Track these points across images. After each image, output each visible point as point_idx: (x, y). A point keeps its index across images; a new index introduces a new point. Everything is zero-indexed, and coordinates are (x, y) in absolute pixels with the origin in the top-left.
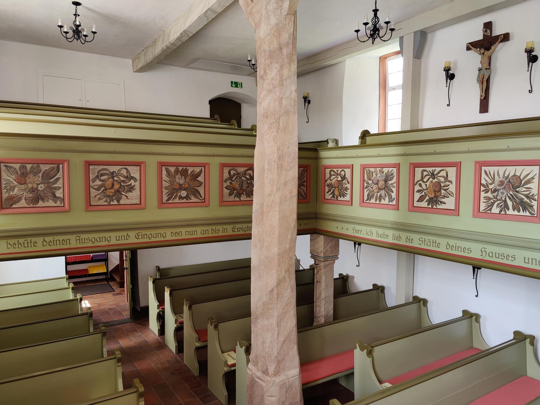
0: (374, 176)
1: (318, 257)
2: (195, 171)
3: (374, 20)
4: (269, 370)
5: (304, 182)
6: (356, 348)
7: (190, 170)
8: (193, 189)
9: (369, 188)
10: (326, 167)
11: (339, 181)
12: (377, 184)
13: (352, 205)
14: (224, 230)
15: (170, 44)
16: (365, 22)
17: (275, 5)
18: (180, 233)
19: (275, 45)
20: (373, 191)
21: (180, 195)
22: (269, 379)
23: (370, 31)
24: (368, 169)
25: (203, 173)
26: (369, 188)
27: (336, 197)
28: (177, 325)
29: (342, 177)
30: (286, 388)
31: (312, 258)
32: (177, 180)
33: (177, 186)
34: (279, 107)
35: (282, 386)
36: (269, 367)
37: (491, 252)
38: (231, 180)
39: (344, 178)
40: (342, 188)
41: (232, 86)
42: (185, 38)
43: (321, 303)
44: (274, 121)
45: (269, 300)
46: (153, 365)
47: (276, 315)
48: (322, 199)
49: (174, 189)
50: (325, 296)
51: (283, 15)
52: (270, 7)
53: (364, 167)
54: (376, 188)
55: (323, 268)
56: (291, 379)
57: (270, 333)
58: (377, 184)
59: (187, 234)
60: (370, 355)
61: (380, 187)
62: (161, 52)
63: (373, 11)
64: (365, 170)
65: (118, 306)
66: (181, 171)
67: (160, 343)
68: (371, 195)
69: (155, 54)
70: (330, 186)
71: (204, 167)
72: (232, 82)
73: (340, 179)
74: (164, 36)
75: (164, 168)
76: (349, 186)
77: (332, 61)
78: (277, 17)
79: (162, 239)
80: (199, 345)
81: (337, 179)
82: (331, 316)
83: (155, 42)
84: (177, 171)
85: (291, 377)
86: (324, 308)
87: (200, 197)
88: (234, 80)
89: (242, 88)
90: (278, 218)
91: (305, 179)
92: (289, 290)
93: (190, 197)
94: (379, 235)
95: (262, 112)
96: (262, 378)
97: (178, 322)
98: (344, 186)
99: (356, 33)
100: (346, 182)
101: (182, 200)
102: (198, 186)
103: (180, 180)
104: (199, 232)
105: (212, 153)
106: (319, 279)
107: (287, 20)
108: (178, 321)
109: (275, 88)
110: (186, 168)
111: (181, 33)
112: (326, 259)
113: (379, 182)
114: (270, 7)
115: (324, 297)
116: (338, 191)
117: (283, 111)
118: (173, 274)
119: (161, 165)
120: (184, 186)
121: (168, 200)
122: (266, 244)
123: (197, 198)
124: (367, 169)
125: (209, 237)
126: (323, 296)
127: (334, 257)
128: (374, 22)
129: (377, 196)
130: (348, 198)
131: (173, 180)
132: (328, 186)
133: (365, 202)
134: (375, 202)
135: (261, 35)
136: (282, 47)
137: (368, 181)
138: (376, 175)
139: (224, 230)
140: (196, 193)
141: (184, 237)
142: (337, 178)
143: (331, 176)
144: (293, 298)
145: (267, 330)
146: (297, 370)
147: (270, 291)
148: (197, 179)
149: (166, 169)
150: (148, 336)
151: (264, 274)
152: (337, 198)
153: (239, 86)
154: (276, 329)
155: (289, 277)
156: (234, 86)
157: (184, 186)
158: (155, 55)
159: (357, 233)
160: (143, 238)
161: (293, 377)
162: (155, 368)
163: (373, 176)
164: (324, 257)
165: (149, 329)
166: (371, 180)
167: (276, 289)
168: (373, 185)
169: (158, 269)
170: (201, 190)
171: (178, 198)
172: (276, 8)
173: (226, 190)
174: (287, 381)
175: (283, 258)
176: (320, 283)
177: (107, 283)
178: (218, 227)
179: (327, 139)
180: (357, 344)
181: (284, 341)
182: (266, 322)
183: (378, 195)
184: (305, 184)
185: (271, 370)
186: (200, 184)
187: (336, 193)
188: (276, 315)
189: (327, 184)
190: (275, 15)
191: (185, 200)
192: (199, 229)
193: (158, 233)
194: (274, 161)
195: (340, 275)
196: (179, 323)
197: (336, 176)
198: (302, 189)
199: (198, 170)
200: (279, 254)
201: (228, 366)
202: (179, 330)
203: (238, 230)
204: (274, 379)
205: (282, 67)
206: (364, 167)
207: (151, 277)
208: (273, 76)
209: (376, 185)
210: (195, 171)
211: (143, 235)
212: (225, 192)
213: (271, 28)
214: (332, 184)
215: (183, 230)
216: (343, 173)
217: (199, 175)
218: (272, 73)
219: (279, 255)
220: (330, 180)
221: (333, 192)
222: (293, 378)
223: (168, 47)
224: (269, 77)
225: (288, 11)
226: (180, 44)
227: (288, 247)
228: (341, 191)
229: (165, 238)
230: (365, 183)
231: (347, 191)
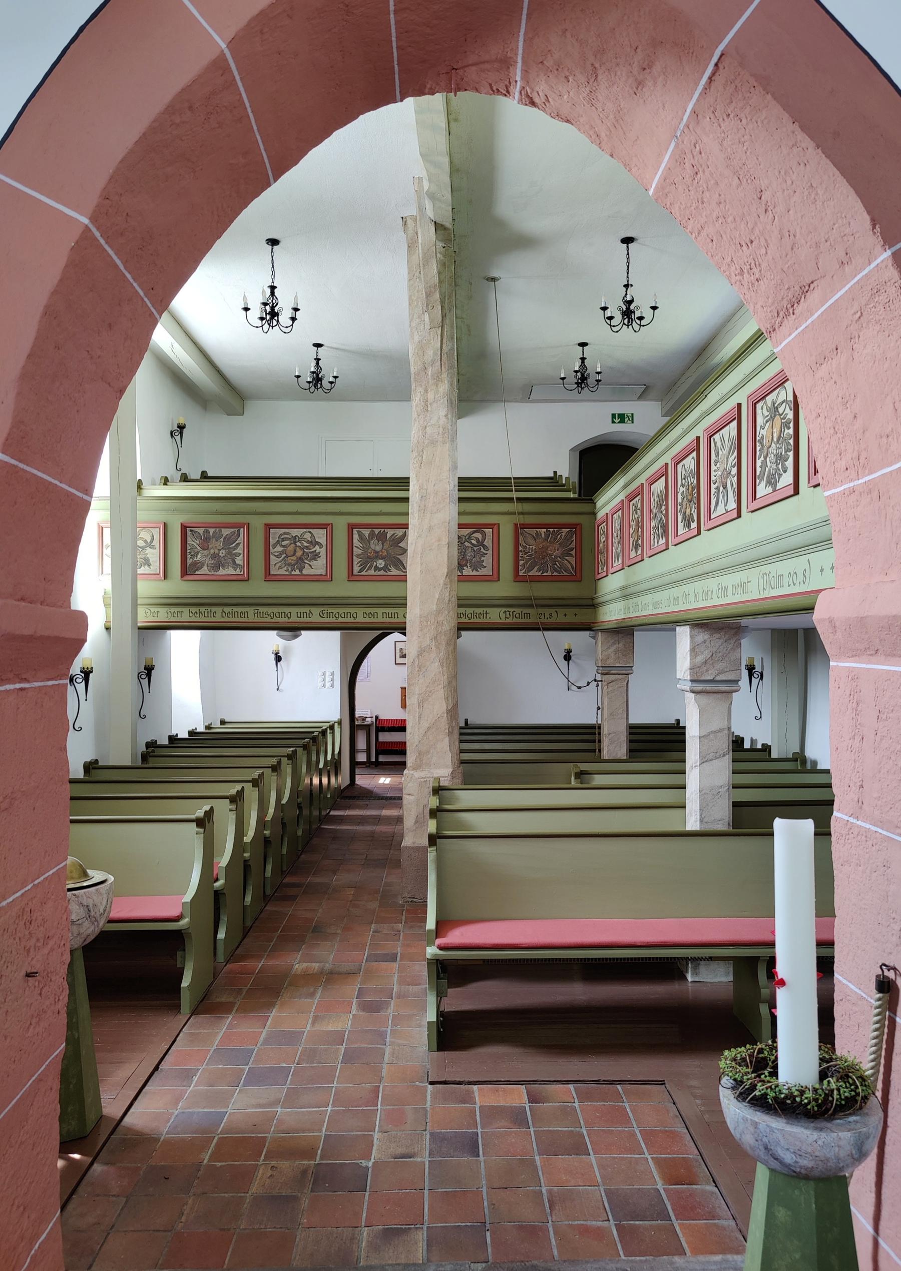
16: (654, 305)
18: (375, 614)
32: (373, 546)
41: (613, 422)
59: (385, 617)
72: (613, 416)
75: (355, 531)
79: (352, 620)
84: (372, 535)
88: (617, 412)
89: (633, 422)
90: (419, 571)
91: (573, 545)
92: (437, 664)
117: (427, 442)
119: (351, 527)
121: (360, 571)
153: (626, 420)
155: (437, 647)
156: (617, 421)
167: (417, 659)
184: (573, 553)
191: (382, 573)
198: (566, 560)
204: (412, 772)
205: (426, 391)
215: (380, 611)
227: (435, 609)
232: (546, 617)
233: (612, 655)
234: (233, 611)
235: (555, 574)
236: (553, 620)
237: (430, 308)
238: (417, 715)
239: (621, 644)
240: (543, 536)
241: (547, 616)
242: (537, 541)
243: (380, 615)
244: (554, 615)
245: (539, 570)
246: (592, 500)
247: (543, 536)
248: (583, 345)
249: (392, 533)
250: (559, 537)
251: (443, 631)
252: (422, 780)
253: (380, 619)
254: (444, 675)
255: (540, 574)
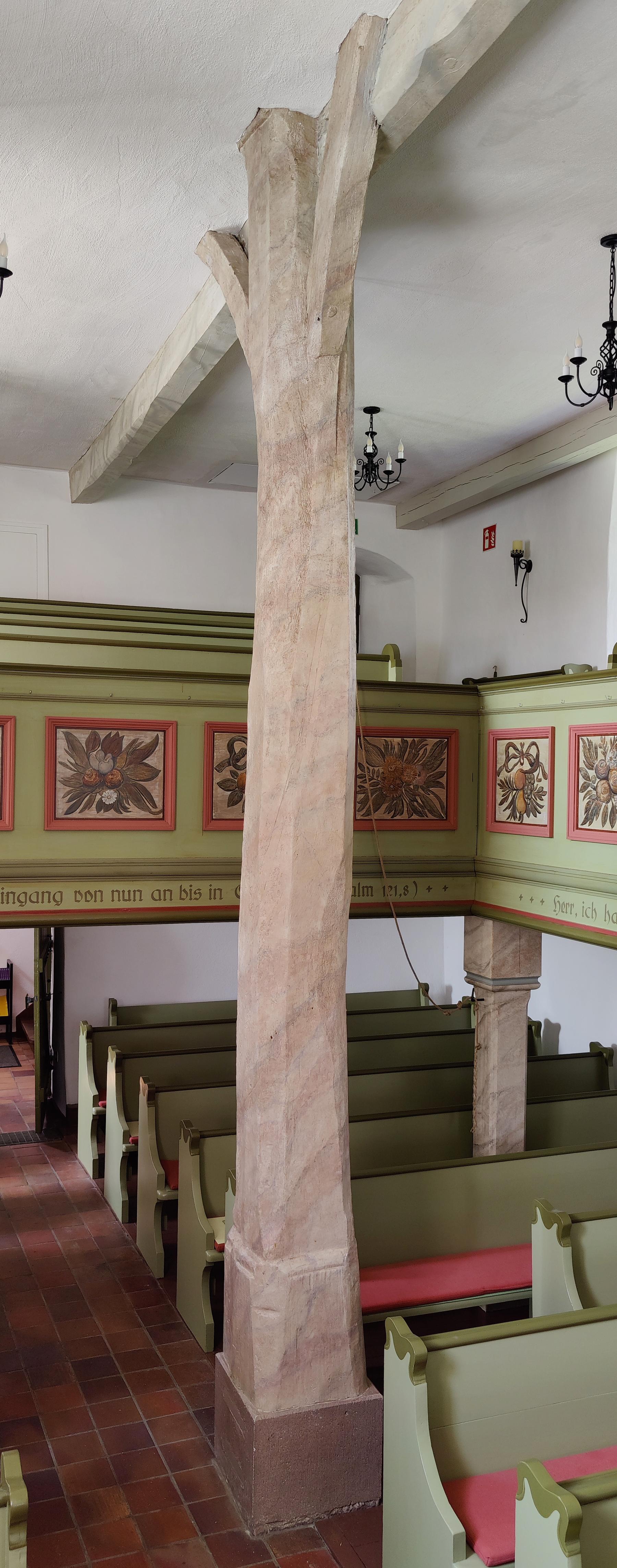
0: (599, 759)
1: (480, 979)
2: (139, 741)
3: (606, 352)
4: (264, 1242)
5: (441, 775)
6: (535, 1221)
7: (128, 738)
8: (135, 785)
9: (588, 790)
10: (498, 737)
11: (526, 772)
12: (606, 778)
13: (551, 836)
14: (212, 894)
15: (134, 432)
16: (577, 355)
17: (291, 335)
18: (99, 894)
19: (292, 430)
20: (598, 798)
21: (101, 801)
22: (262, 1263)
23: (597, 378)
24: (588, 739)
25: (160, 747)
26: (590, 788)
27: (518, 815)
28: (126, 1147)
29: (533, 761)
30: (307, 1292)
31: (468, 982)
32: (94, 764)
33: (94, 776)
34: (299, 578)
35: (297, 1284)
36: (263, 1234)
37: (157, 890)
38: (235, 766)
39: (535, 764)
40: (531, 791)
42: (166, 417)
43: (488, 1108)
44: (285, 612)
45: (267, 1060)
46: (59, 1244)
47: (283, 1100)
48: (487, 821)
49: (86, 785)
50: (498, 1086)
51: (310, 357)
52: (280, 342)
53: (578, 735)
54: (605, 788)
55: (494, 1010)
56: (324, 1271)
57: (268, 1147)
58: (606, 778)
59: (116, 897)
60: (568, 1240)
61: (612, 787)
62: (120, 452)
63: (605, 325)
64: (580, 740)
65: (18, 1102)
66: (104, 740)
67: (94, 1194)
68: (594, 808)
69: (109, 456)
70: (505, 785)
71: (164, 731)
73: (527, 767)
74: (123, 414)
75: (60, 733)
76: (545, 784)
77: (574, 454)
78: (295, 364)
79: (52, 906)
80: (164, 1196)
81: (521, 767)
82: (517, 1144)
83: (107, 428)
84: (93, 742)
85: (324, 1268)
86: (495, 1121)
87: (151, 807)
90: (291, 852)
91: (443, 768)
92: (322, 1039)
93: (127, 805)
94: (609, 915)
95: (262, 591)
96: (249, 1260)
97: (131, 1139)
98: (535, 785)
99: (564, 384)
100: (541, 776)
101: (105, 811)
102: (145, 778)
103: (101, 762)
104: (146, 896)
105: (184, 697)
106: (484, 1041)
107: (320, 369)
108: (130, 1136)
109: (289, 532)
110: (117, 734)
111: (152, 405)
112: (501, 985)
113: (610, 773)
114: (280, 342)
115: (495, 1090)
116: (523, 800)
117: (307, 589)
118: (152, 1019)
119: (54, 724)
120: (110, 777)
121: (70, 810)
122: (263, 918)
123: (144, 808)
124: (585, 738)
125: (162, 908)
126: (493, 1087)
127: (527, 981)
128: (606, 355)
129: (607, 812)
130: (543, 818)
131: (82, 762)
132: (503, 785)
133: (580, 826)
134: (601, 828)
135: (262, 407)
136: (307, 433)
137: (587, 770)
138: (604, 754)
139: (213, 891)
140: (142, 797)
141: (107, 904)
142: (522, 764)
143: (508, 759)
144: (334, 1061)
145: (261, 1137)
146: (342, 1250)
147: (272, 1037)
148: (145, 761)
149: (67, 735)
150: (68, 1177)
151: (257, 994)
152: (520, 817)
154: (285, 1135)
155: (323, 1006)
157: (110, 777)
158: (108, 459)
159: (563, 912)
160: (5, 902)
161: (330, 1266)
162: (62, 1251)
163: (597, 757)
164: (493, 980)
165: (77, 1161)
166: (592, 769)
167: (284, 1032)
168: (597, 782)
169: (114, 1007)
170: (155, 788)
171: (94, 806)
172: (293, 341)
173: (220, 790)
174: (312, 1276)
175: (305, 955)
176: (486, 1052)
177: (7, 1044)
178: (197, 884)
179: (563, 667)
180: (538, 1209)
181: (305, 1169)
182: (259, 1117)
183: (607, 808)
184: (443, 780)
185: (270, 1240)
186: (153, 773)
187: (520, 804)
188: (284, 1099)
189: (501, 781)
190: (290, 360)
191: (111, 814)
192: (148, 888)
193: (43, 893)
194: (285, 712)
195: (593, 1045)
196: (132, 1140)
197: (520, 761)
198: (433, 793)
199: (146, 738)
200: (293, 945)
201: (215, 1249)
202: (130, 1161)
203: (370, 889)
204: (274, 1264)
205: (307, 482)
206: (578, 735)
207: (85, 1023)
208: (284, 504)
209: (604, 781)
210: (139, 741)
211: (5, 894)
212: (217, 797)
213: (282, 388)
214: (510, 781)
215: (107, 887)
216: (533, 751)
217: (149, 750)
218: (284, 497)
219: (293, 947)
220: (506, 771)
221: (513, 802)
222: (328, 1271)
223: (132, 440)
224: (277, 508)
225: (321, 348)
226: (158, 431)
227: (319, 928)
228: (530, 799)
229: (59, 905)
230: (581, 777)
231: (542, 800)
232: (398, 894)
233: (510, 959)
234: (213, 888)
235: (415, 817)
236: (409, 898)
237: (329, 313)
238: (283, 1145)
239: (523, 941)
240: (396, 750)
241: (400, 890)
242: (387, 758)
243: (107, 895)
244: (412, 888)
245: (389, 810)
246: (476, 690)
247: (396, 750)
248: (372, 410)
249: (132, 738)
250: (421, 752)
251: (332, 972)
252: (295, 1278)
253: (107, 904)
254: (334, 1061)
255: (389, 818)
